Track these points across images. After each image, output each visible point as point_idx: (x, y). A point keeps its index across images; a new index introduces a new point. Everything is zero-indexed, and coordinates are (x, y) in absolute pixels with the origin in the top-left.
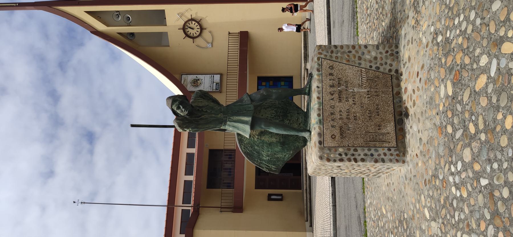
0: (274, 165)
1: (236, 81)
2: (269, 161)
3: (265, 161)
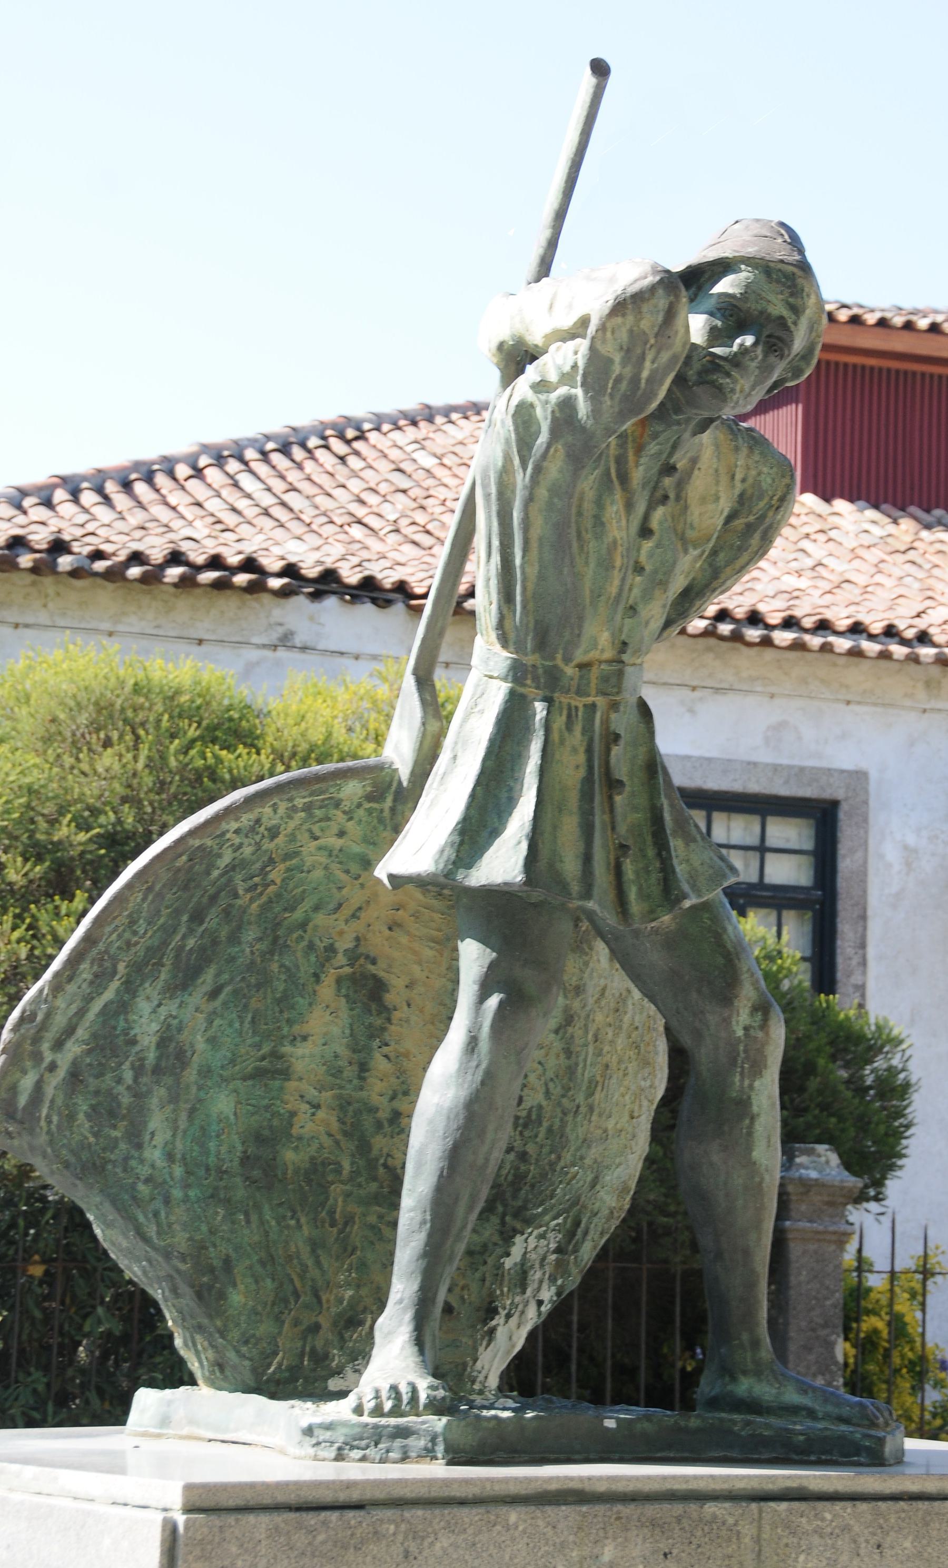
3: (121, 1007)
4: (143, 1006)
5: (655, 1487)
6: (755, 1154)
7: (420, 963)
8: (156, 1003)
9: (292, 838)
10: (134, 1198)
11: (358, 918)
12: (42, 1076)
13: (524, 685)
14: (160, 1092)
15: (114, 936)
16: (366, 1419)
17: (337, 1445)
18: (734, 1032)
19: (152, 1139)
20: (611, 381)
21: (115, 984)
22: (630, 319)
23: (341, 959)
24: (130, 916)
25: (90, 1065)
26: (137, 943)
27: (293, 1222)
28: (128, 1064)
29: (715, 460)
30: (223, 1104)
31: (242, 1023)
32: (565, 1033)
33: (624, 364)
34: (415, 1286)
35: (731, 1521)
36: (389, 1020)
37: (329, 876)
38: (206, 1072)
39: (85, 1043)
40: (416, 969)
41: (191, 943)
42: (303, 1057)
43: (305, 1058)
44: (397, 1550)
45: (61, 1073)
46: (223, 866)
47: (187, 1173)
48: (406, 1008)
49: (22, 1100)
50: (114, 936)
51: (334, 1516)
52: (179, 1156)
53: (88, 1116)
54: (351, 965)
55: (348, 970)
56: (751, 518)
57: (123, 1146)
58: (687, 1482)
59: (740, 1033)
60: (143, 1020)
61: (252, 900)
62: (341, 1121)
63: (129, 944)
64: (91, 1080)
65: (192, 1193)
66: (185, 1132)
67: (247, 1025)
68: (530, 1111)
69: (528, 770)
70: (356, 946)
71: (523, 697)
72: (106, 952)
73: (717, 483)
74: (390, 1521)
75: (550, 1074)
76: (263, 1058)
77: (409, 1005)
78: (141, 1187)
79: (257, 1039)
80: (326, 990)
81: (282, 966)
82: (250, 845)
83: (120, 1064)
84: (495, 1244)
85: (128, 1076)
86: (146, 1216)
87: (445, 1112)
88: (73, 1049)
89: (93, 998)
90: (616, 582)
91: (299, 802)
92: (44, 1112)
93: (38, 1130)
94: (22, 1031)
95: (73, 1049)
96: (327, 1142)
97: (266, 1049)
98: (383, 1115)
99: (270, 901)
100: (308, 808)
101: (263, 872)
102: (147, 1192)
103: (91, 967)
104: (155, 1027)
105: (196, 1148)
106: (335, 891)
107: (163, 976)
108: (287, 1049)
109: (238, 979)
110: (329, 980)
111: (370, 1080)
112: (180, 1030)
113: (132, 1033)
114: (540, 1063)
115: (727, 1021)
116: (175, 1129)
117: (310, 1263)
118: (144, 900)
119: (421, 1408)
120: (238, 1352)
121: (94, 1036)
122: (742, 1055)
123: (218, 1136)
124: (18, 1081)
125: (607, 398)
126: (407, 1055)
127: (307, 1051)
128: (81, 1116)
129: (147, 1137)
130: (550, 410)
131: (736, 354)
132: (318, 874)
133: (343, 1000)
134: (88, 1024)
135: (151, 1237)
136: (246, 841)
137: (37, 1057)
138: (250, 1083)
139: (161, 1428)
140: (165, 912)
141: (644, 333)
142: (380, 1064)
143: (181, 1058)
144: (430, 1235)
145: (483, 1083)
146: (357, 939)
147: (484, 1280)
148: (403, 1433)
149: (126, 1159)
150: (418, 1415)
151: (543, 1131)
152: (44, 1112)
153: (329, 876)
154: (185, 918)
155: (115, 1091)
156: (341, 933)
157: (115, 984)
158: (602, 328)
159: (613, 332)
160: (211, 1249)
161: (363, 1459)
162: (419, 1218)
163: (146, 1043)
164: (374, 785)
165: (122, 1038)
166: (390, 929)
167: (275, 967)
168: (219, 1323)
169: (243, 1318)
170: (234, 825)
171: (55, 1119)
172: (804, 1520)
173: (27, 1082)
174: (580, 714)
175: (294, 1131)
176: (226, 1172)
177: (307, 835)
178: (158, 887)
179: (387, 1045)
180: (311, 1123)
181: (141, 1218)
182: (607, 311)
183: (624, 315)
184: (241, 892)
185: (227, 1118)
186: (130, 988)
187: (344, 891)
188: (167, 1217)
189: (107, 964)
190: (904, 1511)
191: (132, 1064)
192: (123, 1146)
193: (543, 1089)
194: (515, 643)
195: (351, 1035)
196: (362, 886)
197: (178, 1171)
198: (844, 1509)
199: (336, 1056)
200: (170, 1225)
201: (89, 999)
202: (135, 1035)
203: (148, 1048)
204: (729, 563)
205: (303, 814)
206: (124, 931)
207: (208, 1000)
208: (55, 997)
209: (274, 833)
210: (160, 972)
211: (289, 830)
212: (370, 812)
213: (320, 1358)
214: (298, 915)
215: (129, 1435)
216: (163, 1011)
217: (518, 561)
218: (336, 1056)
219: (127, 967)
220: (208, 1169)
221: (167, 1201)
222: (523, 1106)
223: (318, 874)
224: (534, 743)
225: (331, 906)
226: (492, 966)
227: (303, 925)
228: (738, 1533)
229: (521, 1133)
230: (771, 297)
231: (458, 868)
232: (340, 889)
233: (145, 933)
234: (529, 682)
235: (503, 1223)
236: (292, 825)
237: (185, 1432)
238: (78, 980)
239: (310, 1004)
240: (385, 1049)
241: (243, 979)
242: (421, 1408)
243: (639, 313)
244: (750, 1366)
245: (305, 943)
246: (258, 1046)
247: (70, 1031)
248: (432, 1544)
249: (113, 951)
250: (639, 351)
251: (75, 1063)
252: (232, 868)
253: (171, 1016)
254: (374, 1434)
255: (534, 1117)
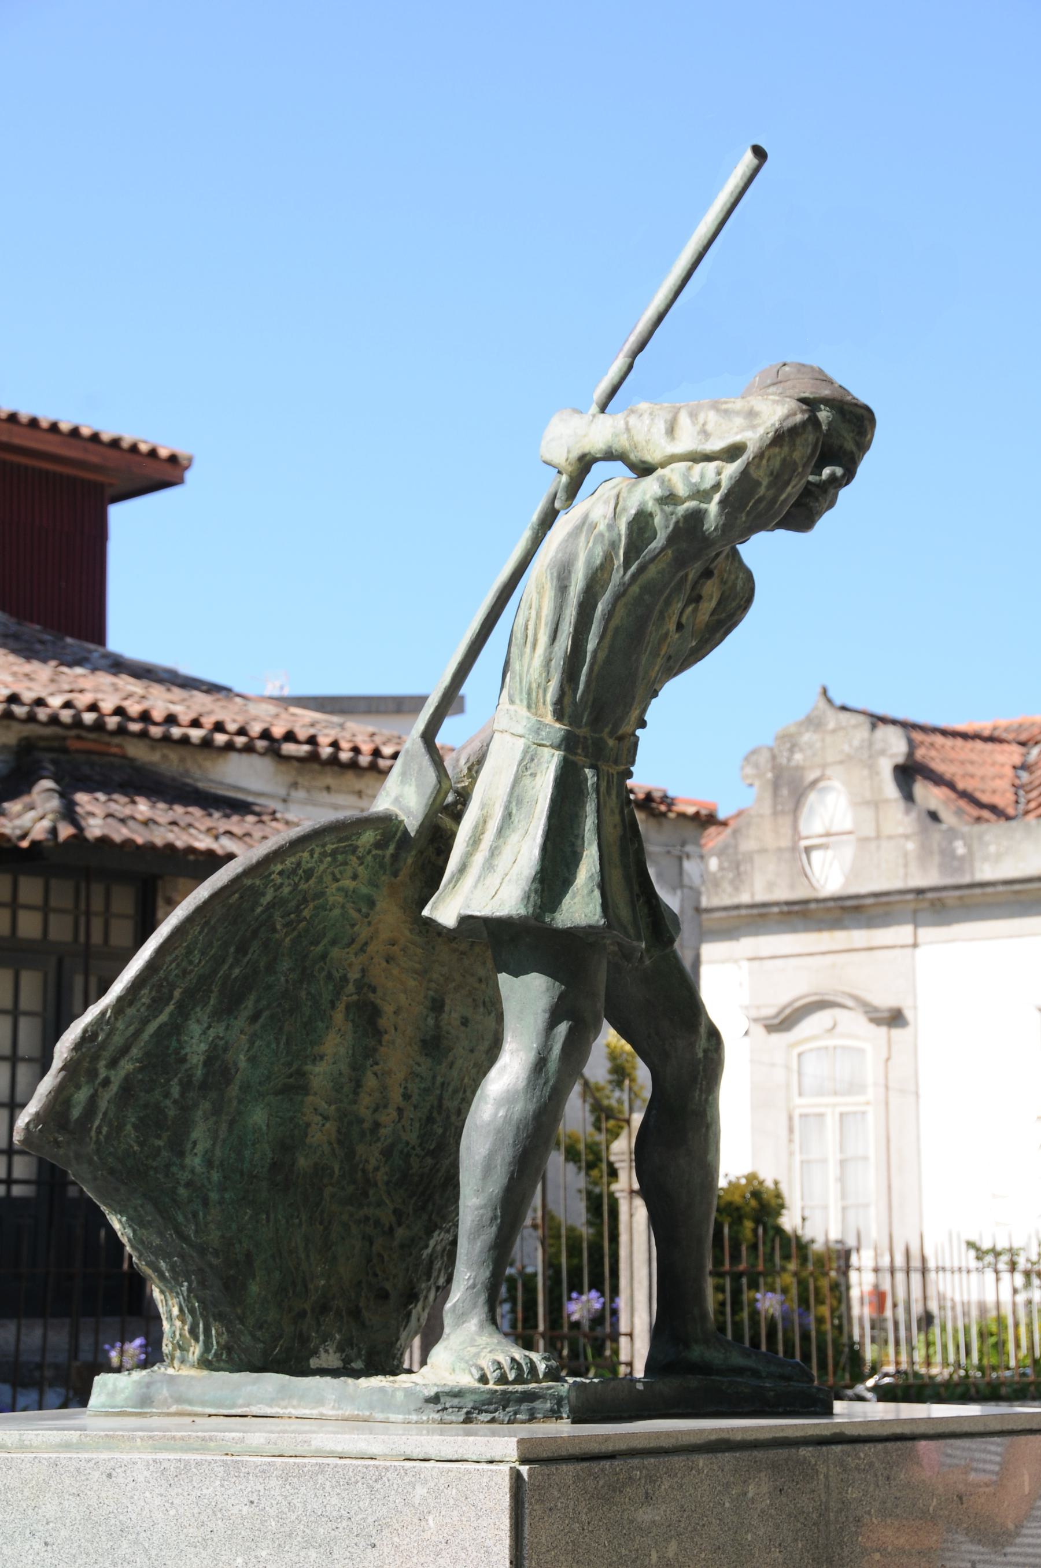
3: (175, 1029)
4: (195, 1028)
5: (768, 1435)
7: (405, 992)
8: (206, 1025)
9: (320, 879)
10: (174, 1201)
11: (365, 952)
12: (96, 1091)
13: (576, 754)
14: (206, 1105)
15: (174, 965)
16: (491, 1386)
17: (465, 1410)
18: (697, 1054)
19: (194, 1147)
20: (753, 501)
21: (170, 1008)
22: (786, 449)
23: (351, 988)
24: (188, 947)
25: (141, 1080)
26: (192, 971)
27: (297, 1221)
28: (176, 1080)
30: (258, 1116)
31: (278, 1044)
33: (768, 488)
34: (488, 1274)
35: (813, 1462)
36: (380, 1042)
37: (344, 914)
38: (246, 1088)
39: (137, 1060)
40: (402, 997)
41: (236, 971)
42: (319, 1074)
43: (320, 1074)
44: (641, 1491)
45: (114, 1088)
46: (265, 903)
47: (224, 1177)
48: (393, 1031)
49: (76, 1113)
50: (174, 965)
51: (606, 1464)
52: (217, 1163)
53: (136, 1127)
54: (358, 993)
55: (355, 997)
57: (165, 1154)
58: (783, 1430)
59: (701, 1055)
60: (194, 1041)
61: (287, 934)
62: (339, 1131)
63: (185, 972)
64: (142, 1094)
65: (227, 1196)
66: (224, 1141)
67: (282, 1046)
69: (587, 828)
70: (363, 976)
71: (574, 764)
72: (166, 979)
74: (638, 1468)
76: (290, 1076)
77: (396, 1029)
78: (182, 1191)
79: (289, 1058)
80: (339, 1016)
81: (309, 993)
82: (289, 885)
83: (169, 1080)
84: (421, 1238)
85: (176, 1091)
86: (185, 1217)
87: (514, 1122)
88: (127, 1066)
89: (149, 1021)
91: (329, 848)
92: (97, 1123)
93: (88, 1140)
94: (84, 1050)
95: (127, 1066)
96: (326, 1148)
97: (294, 1067)
98: (367, 1125)
99: (299, 936)
100: (334, 853)
101: (298, 910)
102: (186, 1195)
103: (150, 993)
104: (203, 1047)
105: (233, 1155)
106: (348, 927)
107: (212, 1002)
108: (309, 1067)
109: (275, 1005)
110: (341, 1007)
111: (362, 1095)
112: (225, 1050)
113: (183, 1052)
115: (692, 1045)
116: (215, 1138)
117: (303, 1256)
118: (200, 933)
119: (541, 1376)
120: (253, 1336)
121: (147, 1054)
122: (701, 1073)
123: (253, 1145)
124: (72, 1095)
125: (744, 515)
126: (390, 1072)
127: (322, 1069)
128: (129, 1127)
129: (189, 1146)
130: (674, 519)
131: (824, 482)
132: (337, 912)
133: (350, 1024)
134: (142, 1044)
135: (189, 1236)
136: (286, 882)
137: (93, 1074)
138: (280, 1097)
139: (141, 1407)
140: (216, 944)
141: (795, 462)
142: (370, 1082)
143: (226, 1074)
144: (500, 1229)
145: (550, 1098)
146: (363, 971)
147: (407, 1270)
148: (530, 1397)
149: (168, 1166)
150: (538, 1381)
152: (97, 1123)
153: (344, 914)
154: (232, 949)
155: (162, 1105)
156: (350, 965)
157: (170, 1008)
158: (760, 456)
159: (768, 461)
160: (237, 1246)
161: (493, 1421)
162: (490, 1214)
163: (195, 1061)
164: (383, 835)
165: (173, 1056)
166: (388, 962)
167: (303, 994)
168: (239, 1311)
169: (257, 1306)
170: (279, 867)
171: (105, 1130)
172: (850, 1459)
173: (81, 1096)
175: (308, 1140)
176: (255, 1177)
177: (330, 877)
178: (212, 922)
179: (377, 1064)
180: (320, 1133)
181: (180, 1218)
182: (768, 442)
183: (781, 446)
184: (278, 927)
185: (260, 1129)
186: (183, 1012)
187: (356, 928)
188: (205, 1217)
189: (165, 990)
190: (900, 1449)
191: (180, 1080)
192: (165, 1154)
194: (570, 717)
195: (353, 1055)
196: (369, 923)
197: (215, 1176)
198: (870, 1449)
199: (340, 1074)
200: (206, 1225)
201: (145, 1022)
202: (186, 1054)
203: (197, 1065)
205: (329, 859)
206: (182, 960)
207: (250, 1023)
208: (116, 1019)
209: (309, 874)
210: (209, 997)
212: (375, 857)
213: (303, 1339)
214: (319, 948)
215: (90, 1416)
216: (212, 1033)
217: (591, 646)
218: (340, 1074)
219: (182, 993)
220: (242, 1174)
221: (205, 1202)
223: (337, 912)
224: (588, 804)
225: (345, 941)
226: (562, 997)
227: (324, 957)
228: (817, 1471)
230: (845, 435)
231: (544, 912)
232: (353, 926)
233: (200, 962)
234: (579, 751)
235: (430, 1220)
236: (322, 868)
237: (174, 1409)
238: (139, 1004)
239: (327, 1028)
240: (376, 1068)
241: (279, 1005)
242: (541, 1376)
243: (793, 447)
245: (324, 974)
246: (289, 1064)
247: (125, 1050)
248: (659, 1486)
249: (171, 978)
250: (786, 477)
251: (127, 1078)
252: (272, 905)
253: (218, 1037)
254: (502, 1400)
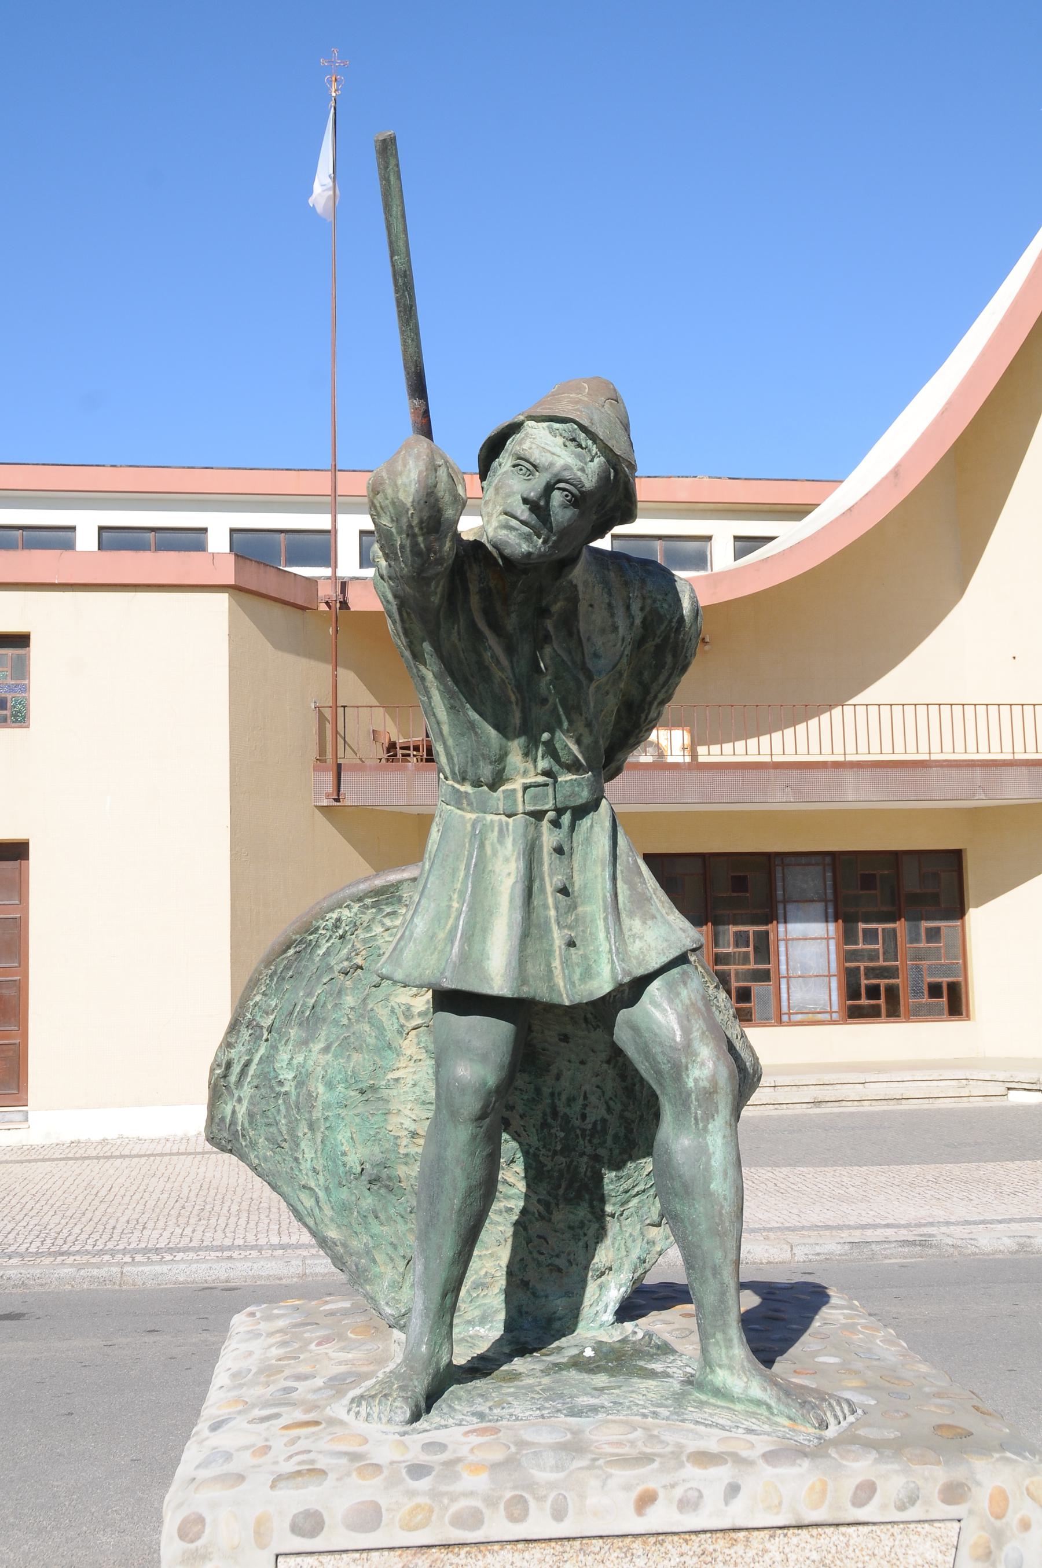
0: (251, 1115)
1: (1019, 748)
2: (268, 1081)
3: (268, 1059)
6: (712, 1186)
29: (606, 596)
32: (617, 1062)
56: (658, 641)
68: (595, 1124)
73: (613, 615)
75: (609, 1094)
90: (518, 715)
114: (598, 1087)
151: (609, 1138)
174: (510, 828)
193: (605, 1106)
204: (655, 678)
211: (365, 924)
222: (588, 1120)
229: (590, 1141)
244: (725, 1361)
255: (599, 1128)
